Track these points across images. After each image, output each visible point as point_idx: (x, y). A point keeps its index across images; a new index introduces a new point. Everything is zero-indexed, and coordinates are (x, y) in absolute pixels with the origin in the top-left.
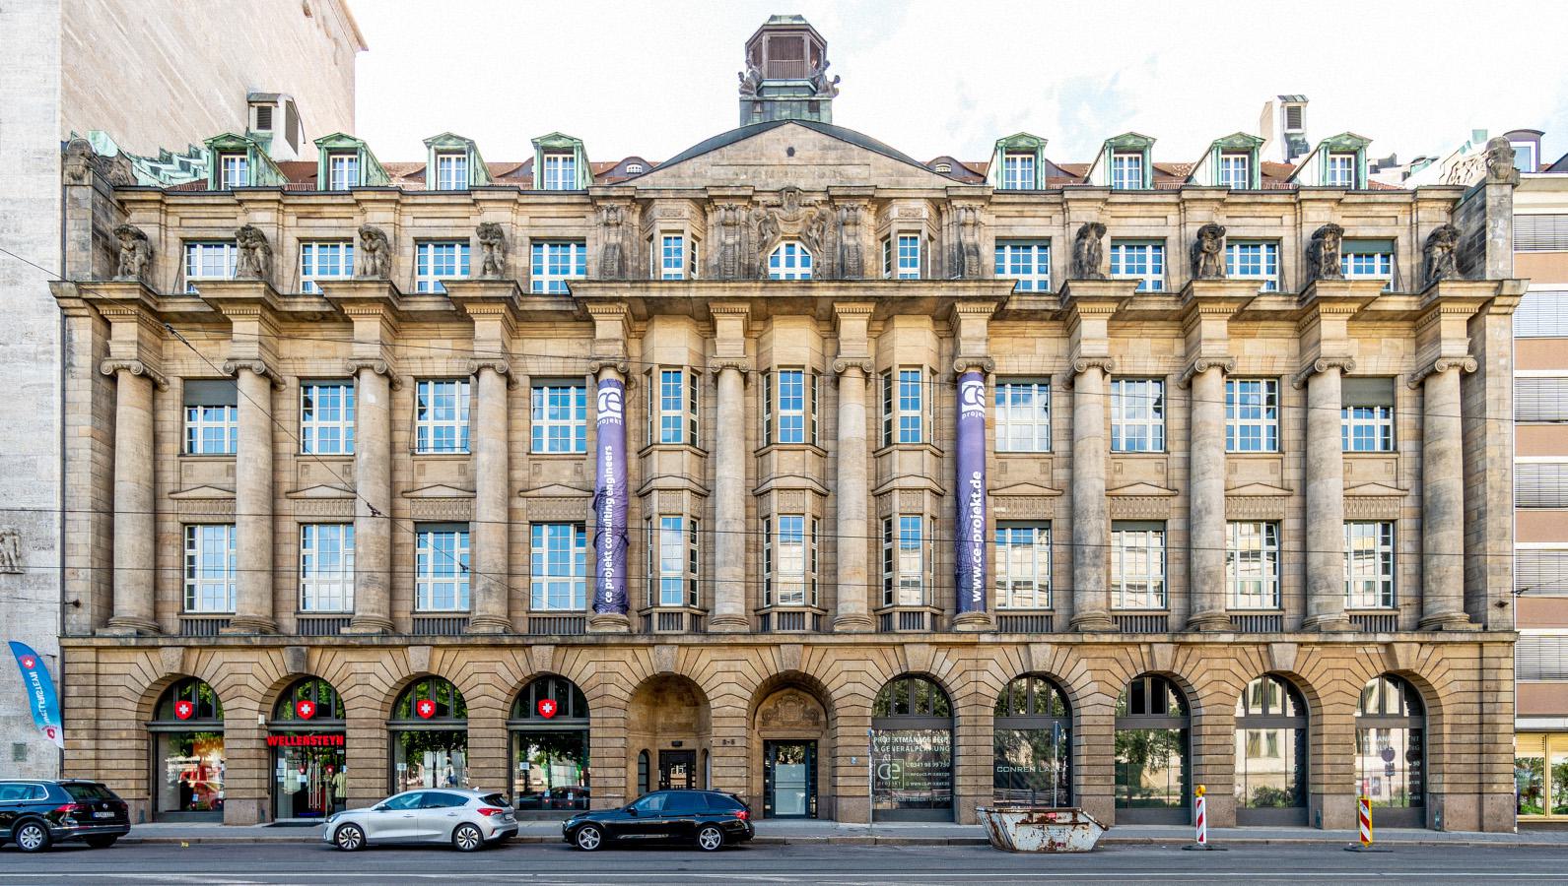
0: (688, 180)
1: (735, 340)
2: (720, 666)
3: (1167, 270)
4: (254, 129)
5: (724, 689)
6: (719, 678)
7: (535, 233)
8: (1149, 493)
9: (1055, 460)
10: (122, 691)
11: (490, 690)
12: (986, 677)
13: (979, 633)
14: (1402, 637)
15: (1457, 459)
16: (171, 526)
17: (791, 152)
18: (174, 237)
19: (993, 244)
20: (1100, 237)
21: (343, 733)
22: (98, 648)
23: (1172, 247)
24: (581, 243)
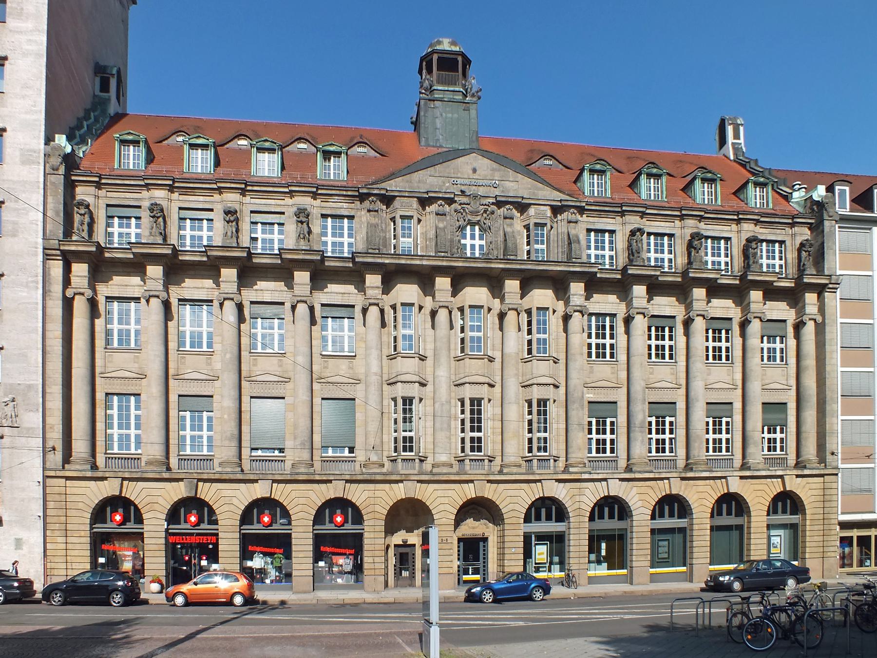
0: (416, 185)
1: (447, 290)
2: (439, 493)
3: (675, 252)
4: (98, 92)
5: (442, 507)
6: (439, 501)
7: (324, 212)
8: (668, 386)
9: (619, 366)
10: (81, 506)
11: (306, 508)
12: (584, 499)
13: (581, 473)
14: (788, 472)
15: (725, 399)
16: (100, 396)
17: (474, 171)
18: (102, 203)
19: (585, 232)
20: (642, 236)
21: (217, 535)
22: (68, 478)
23: (678, 241)
24: (351, 218)
